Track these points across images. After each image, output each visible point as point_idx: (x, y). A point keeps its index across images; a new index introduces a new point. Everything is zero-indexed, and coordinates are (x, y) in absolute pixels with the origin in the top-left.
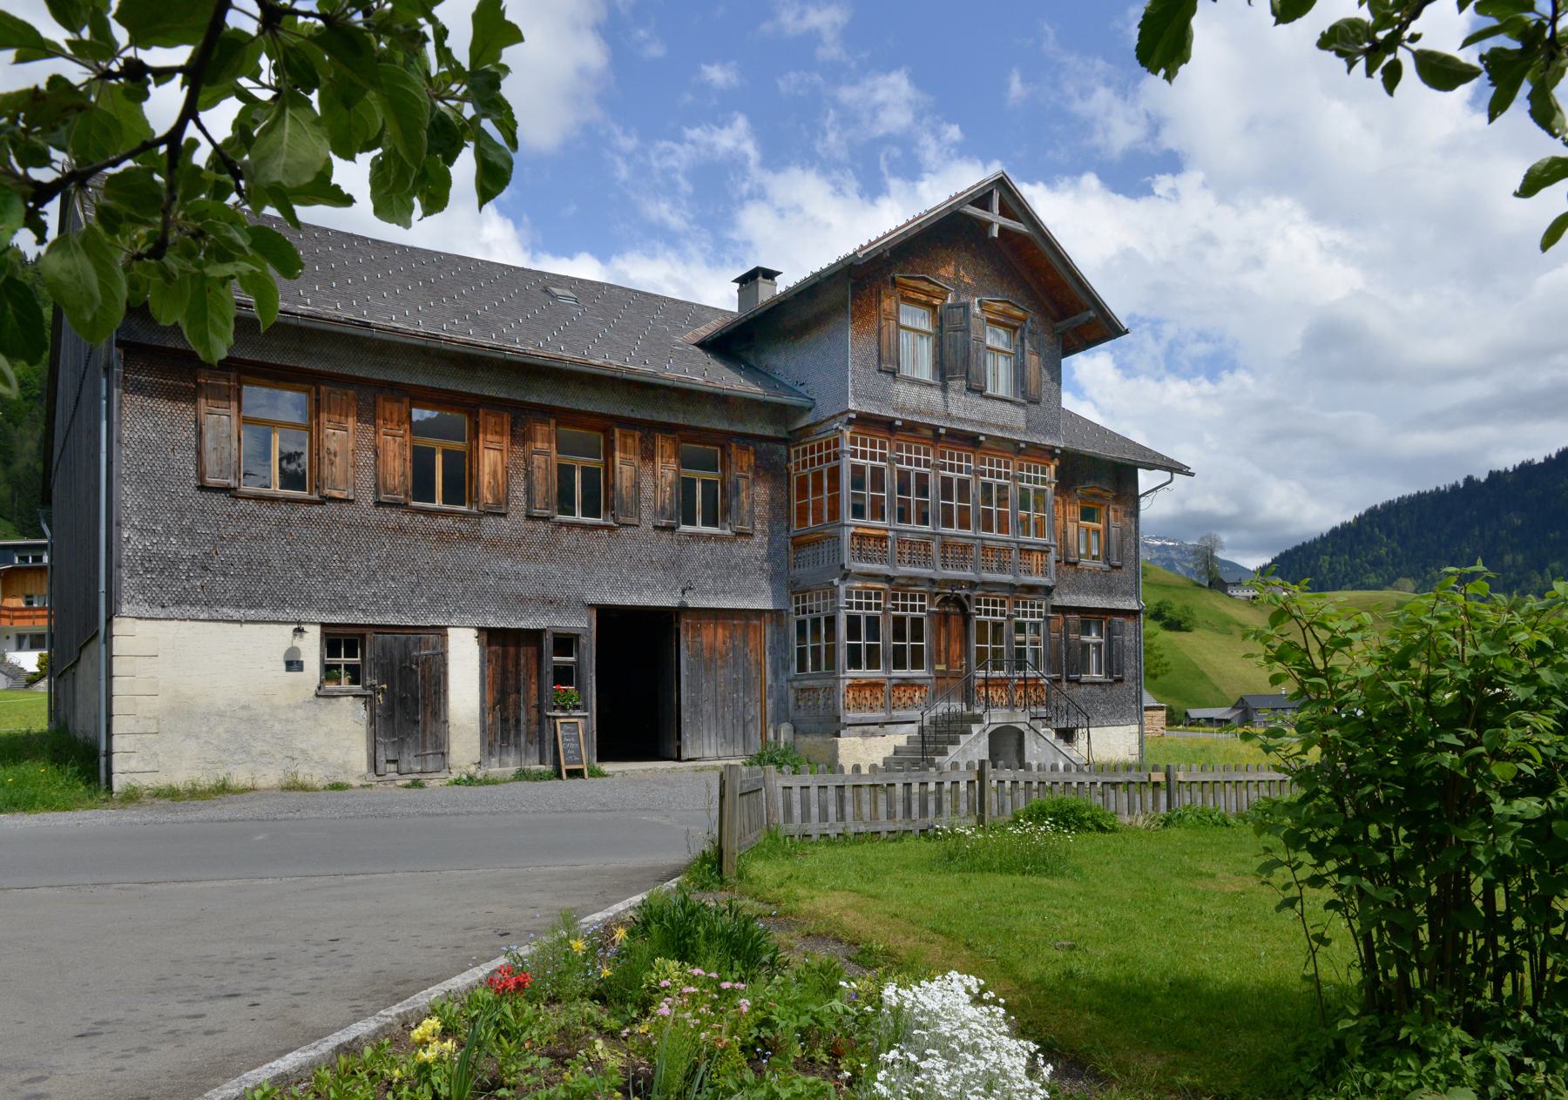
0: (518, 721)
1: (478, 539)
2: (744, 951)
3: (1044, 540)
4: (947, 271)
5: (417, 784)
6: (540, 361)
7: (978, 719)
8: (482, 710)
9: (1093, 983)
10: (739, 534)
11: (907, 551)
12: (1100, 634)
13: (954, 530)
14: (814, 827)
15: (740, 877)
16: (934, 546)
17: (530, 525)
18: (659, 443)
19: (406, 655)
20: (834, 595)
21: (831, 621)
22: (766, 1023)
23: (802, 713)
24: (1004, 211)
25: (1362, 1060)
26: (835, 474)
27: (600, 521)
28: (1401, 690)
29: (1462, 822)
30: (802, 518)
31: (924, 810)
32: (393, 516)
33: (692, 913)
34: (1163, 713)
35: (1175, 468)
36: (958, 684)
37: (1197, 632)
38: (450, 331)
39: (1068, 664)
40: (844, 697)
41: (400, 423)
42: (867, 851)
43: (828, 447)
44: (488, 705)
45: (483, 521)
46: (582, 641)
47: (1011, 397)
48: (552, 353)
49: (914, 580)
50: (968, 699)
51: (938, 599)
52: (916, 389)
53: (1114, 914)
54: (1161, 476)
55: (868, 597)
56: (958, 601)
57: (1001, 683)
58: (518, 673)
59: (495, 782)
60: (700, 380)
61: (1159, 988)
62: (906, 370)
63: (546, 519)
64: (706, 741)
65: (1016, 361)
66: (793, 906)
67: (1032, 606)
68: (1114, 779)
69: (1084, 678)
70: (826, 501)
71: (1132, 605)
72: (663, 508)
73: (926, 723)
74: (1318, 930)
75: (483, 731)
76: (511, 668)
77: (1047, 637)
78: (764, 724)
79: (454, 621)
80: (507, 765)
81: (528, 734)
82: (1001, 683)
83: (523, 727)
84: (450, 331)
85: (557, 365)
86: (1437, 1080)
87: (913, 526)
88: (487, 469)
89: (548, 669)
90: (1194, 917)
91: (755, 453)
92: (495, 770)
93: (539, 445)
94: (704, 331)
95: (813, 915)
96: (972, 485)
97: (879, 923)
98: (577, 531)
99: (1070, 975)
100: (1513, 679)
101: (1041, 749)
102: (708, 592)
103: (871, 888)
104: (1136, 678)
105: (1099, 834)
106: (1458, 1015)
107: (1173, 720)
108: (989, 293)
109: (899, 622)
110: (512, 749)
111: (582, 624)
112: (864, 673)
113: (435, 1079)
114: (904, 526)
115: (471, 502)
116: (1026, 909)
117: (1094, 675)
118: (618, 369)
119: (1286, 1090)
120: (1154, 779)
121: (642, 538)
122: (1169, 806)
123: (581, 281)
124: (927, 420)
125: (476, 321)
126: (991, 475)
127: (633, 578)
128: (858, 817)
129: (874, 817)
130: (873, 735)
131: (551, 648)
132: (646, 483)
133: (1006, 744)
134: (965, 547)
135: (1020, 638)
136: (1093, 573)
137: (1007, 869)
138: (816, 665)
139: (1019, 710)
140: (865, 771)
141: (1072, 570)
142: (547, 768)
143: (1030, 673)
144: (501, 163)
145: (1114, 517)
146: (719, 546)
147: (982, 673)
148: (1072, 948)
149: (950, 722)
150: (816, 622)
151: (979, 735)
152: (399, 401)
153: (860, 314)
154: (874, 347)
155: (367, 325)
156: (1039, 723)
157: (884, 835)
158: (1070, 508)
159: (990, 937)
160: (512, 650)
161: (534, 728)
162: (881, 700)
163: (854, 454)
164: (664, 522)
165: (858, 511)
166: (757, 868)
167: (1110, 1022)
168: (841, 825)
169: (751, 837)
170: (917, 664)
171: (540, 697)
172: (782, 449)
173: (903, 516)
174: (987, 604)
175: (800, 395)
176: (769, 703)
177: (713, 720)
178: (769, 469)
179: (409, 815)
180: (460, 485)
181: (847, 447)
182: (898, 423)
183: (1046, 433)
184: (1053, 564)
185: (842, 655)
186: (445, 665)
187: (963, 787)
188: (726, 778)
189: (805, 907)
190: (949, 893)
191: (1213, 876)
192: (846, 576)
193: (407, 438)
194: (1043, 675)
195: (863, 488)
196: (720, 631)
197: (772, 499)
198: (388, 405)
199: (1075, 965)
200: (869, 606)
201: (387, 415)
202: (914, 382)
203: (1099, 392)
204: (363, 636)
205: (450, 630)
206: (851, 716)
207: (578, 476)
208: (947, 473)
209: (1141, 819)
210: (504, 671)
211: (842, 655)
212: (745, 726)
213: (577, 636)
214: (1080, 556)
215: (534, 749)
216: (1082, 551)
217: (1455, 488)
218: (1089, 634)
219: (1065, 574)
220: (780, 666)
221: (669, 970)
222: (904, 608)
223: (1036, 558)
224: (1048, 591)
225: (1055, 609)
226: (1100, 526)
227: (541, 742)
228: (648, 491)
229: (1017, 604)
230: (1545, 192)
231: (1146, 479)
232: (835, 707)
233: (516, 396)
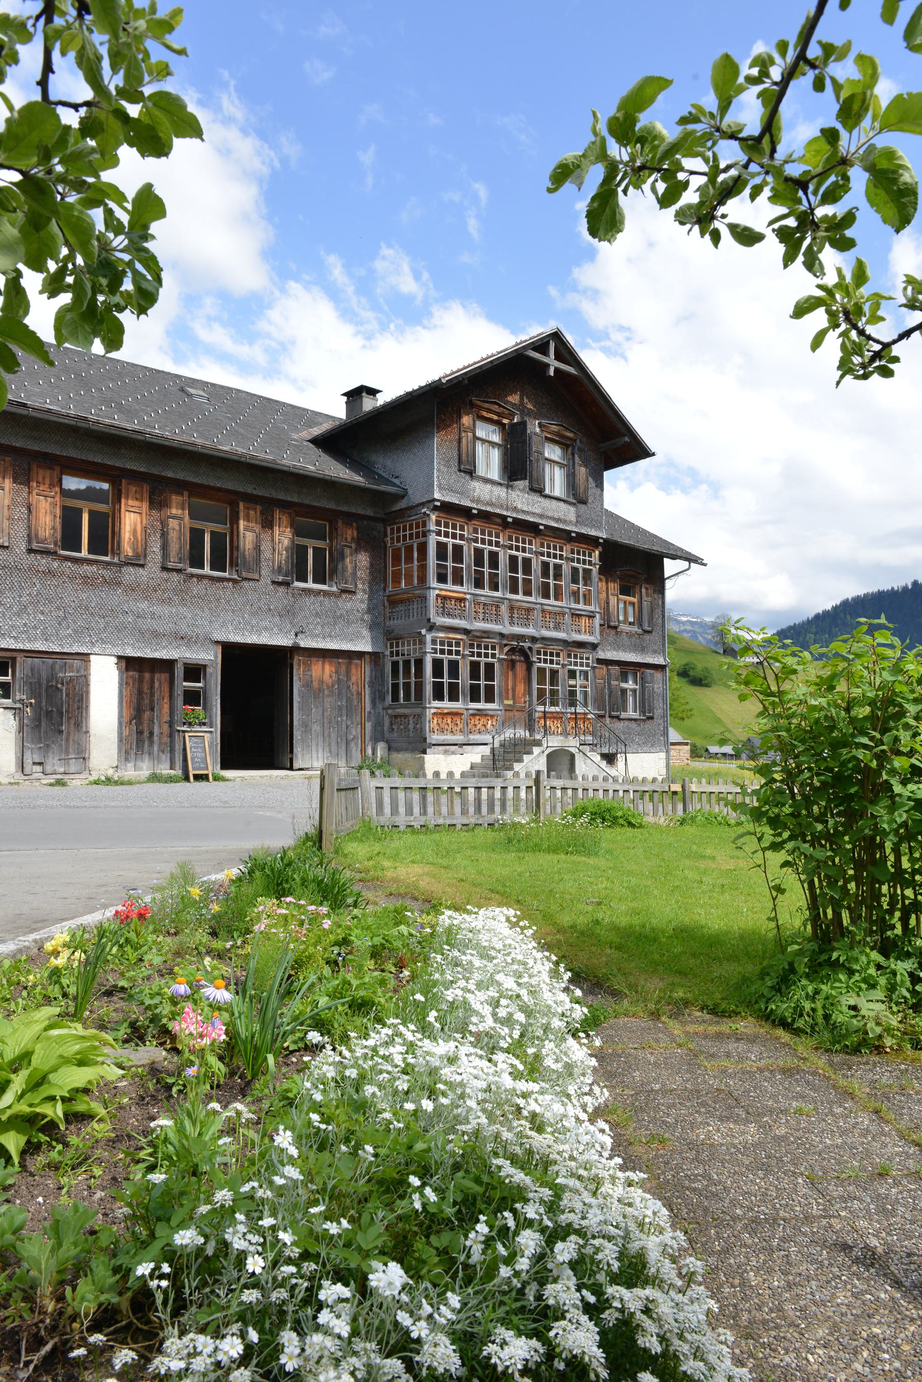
0: (151, 733)
1: (119, 584)
2: (332, 894)
3: (592, 608)
4: (514, 399)
5: (60, 783)
6: (175, 444)
7: (538, 743)
8: (120, 723)
9: (614, 928)
10: (344, 591)
11: (481, 611)
12: (635, 682)
13: (520, 597)
14: (402, 820)
15: (337, 852)
16: (504, 609)
17: (165, 575)
18: (277, 515)
19: (52, 676)
20: (422, 642)
21: (420, 663)
22: (345, 942)
23: (395, 735)
24: (558, 357)
25: (807, 976)
26: (423, 548)
27: (226, 575)
28: (829, 704)
29: (873, 802)
30: (397, 581)
31: (491, 809)
32: (43, 562)
33: (289, 864)
34: (688, 748)
35: (692, 559)
36: (524, 715)
37: (715, 688)
38: (98, 415)
39: (610, 705)
40: (431, 723)
41: (52, 486)
42: (445, 838)
43: (418, 527)
44: (125, 720)
45: (124, 569)
46: (209, 670)
47: (563, 497)
48: (185, 438)
49: (487, 634)
50: (531, 728)
51: (506, 649)
52: (489, 486)
53: (634, 881)
54: (682, 564)
55: (450, 645)
56: (522, 651)
57: (557, 716)
58: (152, 694)
59: (130, 783)
60: (312, 468)
61: (663, 932)
62: (481, 471)
63: (179, 571)
64: (314, 755)
65: (568, 470)
67: (582, 658)
68: (647, 793)
69: (623, 715)
70: (415, 568)
71: (659, 660)
72: (280, 567)
73: (497, 745)
74: (777, 882)
75: (120, 740)
76: (146, 689)
78: (363, 742)
79: (96, 650)
80: (141, 769)
81: (160, 743)
82: (557, 716)
83: (156, 739)
84: (98, 415)
85: (190, 448)
86: (860, 988)
87: (486, 591)
88: (128, 528)
90: (695, 885)
91: (357, 529)
92: (129, 772)
93: (174, 511)
94: (316, 431)
95: (395, 880)
96: (534, 562)
97: (449, 885)
98: (205, 581)
99: (597, 922)
100: (908, 700)
101: (589, 766)
102: (317, 636)
103: (444, 862)
104: (664, 716)
105: (630, 829)
106: (876, 942)
107: (695, 753)
108: (548, 418)
109: (475, 666)
110: (146, 757)
111: (210, 657)
113: (65, 981)
114: (479, 591)
115: (113, 553)
116: (566, 877)
117: (631, 713)
118: (242, 455)
119: (753, 1001)
120: (673, 789)
121: (262, 590)
122: (685, 810)
123: (213, 385)
124: (498, 511)
125: (120, 408)
126: (549, 556)
127: (254, 622)
128: (437, 812)
129: (451, 813)
130: (453, 753)
131: (182, 675)
132: (266, 547)
133: (560, 762)
134: (528, 610)
135: (572, 682)
136: (630, 635)
137: (554, 850)
138: (407, 697)
140: (443, 776)
141: (613, 632)
142: (178, 772)
143: (580, 709)
144: (150, 288)
145: (646, 594)
146: (326, 600)
148: (599, 904)
149: (515, 745)
150: (407, 663)
151: (539, 755)
152: (51, 468)
153: (443, 425)
154: (455, 453)
155: (24, 405)
156: (588, 748)
157: (459, 827)
158: (611, 585)
159: (536, 895)
160: (147, 676)
161: (166, 739)
162: (460, 726)
163: (439, 533)
164: (281, 578)
165: (442, 578)
166: (351, 847)
167: (625, 956)
168: (423, 818)
169: (348, 825)
170: (490, 699)
171: (172, 714)
172: (380, 526)
173: (479, 584)
174: (545, 654)
175: (395, 485)
176: (368, 725)
177: (320, 738)
178: (371, 541)
179: (52, 807)
180: (104, 538)
181: (433, 527)
182: (475, 512)
183: (593, 526)
184: (598, 626)
185: (429, 689)
187: (523, 794)
188: (326, 774)
189: (389, 874)
190: (507, 866)
191: (714, 858)
192: (432, 628)
193: (58, 499)
194: (591, 712)
195: (446, 560)
196: (327, 667)
197: (372, 565)
198: (41, 472)
199: (600, 916)
200: (450, 652)
201: (40, 479)
202: (487, 481)
203: (631, 498)
204: (14, 659)
205: (92, 657)
206: (435, 737)
207: (207, 538)
208: (514, 552)
209: (662, 819)
210: (140, 692)
211: (429, 689)
212: (347, 744)
213: (205, 666)
214: (619, 621)
215: (165, 757)
216: (621, 618)
217: (905, 589)
218: (626, 682)
220: (378, 696)
221: (265, 904)
222: (479, 655)
223: (584, 621)
224: (594, 646)
225: (600, 661)
226: (635, 600)
227: (172, 751)
228: (266, 554)
229: (569, 656)
230: (807, 317)
231: (670, 566)
232: (422, 730)
233: (155, 471)
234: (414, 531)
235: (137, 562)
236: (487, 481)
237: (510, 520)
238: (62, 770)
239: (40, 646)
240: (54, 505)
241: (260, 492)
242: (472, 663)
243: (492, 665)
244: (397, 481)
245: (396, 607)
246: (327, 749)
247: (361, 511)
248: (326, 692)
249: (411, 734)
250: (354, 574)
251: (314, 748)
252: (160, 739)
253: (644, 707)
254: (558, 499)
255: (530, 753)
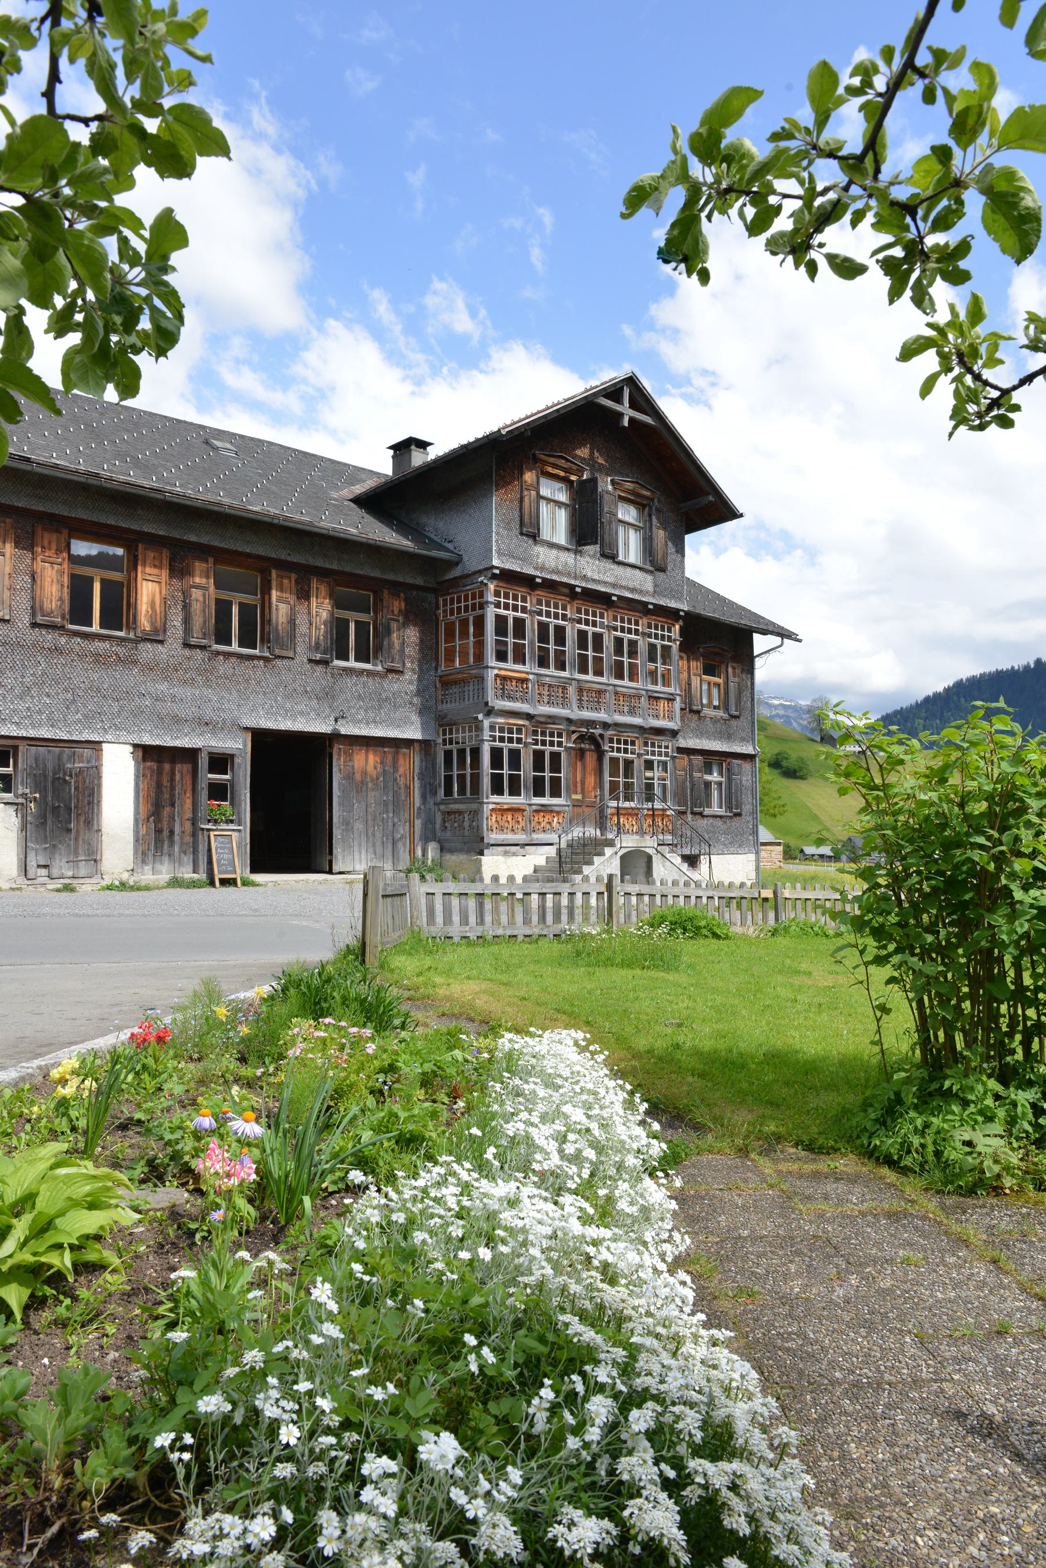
0: (172, 832)
1: (135, 662)
2: (377, 1014)
3: (671, 690)
4: (583, 452)
5: (68, 888)
6: (199, 504)
7: (611, 843)
8: (136, 821)
9: (697, 1053)
10: (390, 671)
11: (546, 693)
12: (721, 774)
13: (590, 677)
14: (456, 930)
15: (382, 967)
16: (572, 690)
17: (187, 652)
18: (314, 584)
19: (59, 767)
20: (479, 728)
21: (476, 752)
22: (391, 1069)
23: (449, 834)
24: (633, 405)
25: (916, 1107)
26: (480, 622)
27: (257, 652)
28: (940, 799)
30: (450, 659)
32: (49, 638)
33: (328, 981)
34: (780, 848)
35: (784, 634)
36: (594, 812)
37: (811, 780)
38: (111, 471)
39: (692, 800)
40: (489, 820)
41: (59, 551)
42: (505, 951)
45: (141, 646)
46: (237, 760)
47: (639, 563)
48: (210, 497)
49: (552, 719)
50: (602, 826)
51: (574, 736)
52: (554, 552)
53: (719, 1000)
54: (774, 640)
55: (511, 731)
56: (592, 739)
57: (632, 813)
58: (172, 788)
59: (147, 888)
60: (354, 531)
61: (752, 1057)
62: (545, 534)
63: (203, 648)
64: (357, 857)
66: (431, 991)
67: (660, 747)
68: (735, 900)
69: (707, 811)
70: (471, 644)
71: (748, 749)
72: (317, 644)
73: (563, 845)
74: (882, 1000)
75: (137, 840)
76: (166, 783)
77: (675, 778)
78: (412, 842)
80: (160, 873)
82: (632, 813)
83: (177, 838)
84: (111, 471)
85: (216, 508)
86: (976, 1121)
87: (552, 671)
88: (145, 599)
89: (203, 786)
90: (789, 1004)
91: (405, 600)
92: (147, 876)
93: (197, 580)
94: (359, 489)
95: (448, 998)
96: (606, 638)
97: (509, 1004)
98: (233, 660)
99: (677, 1046)
100: (1030, 794)
101: (668, 869)
102: (360, 721)
103: (504, 978)
104: (753, 813)
105: (715, 941)
106: (993, 1069)
107: (789, 855)
108: (621, 474)
109: (539, 756)
110: (166, 858)
111: (238, 745)
112: (506, 799)
113: (73, 1113)
114: (543, 671)
115: (128, 628)
116: (642, 995)
117: (715, 809)
118: (274, 517)
119: (855, 1135)
120: (763, 895)
122: (777, 919)
123: (242, 437)
124: (565, 580)
125: (137, 463)
126: (623, 631)
127: (288, 705)
128: (496, 922)
129: (512, 922)
130: (514, 854)
131: (206, 766)
132: (301, 620)
133: (636, 864)
134: (600, 692)
135: (649, 774)
136: (714, 720)
137: (628, 964)
138: (462, 791)
139: (648, 837)
140: (503, 880)
141: (695, 717)
142: (202, 876)
143: (658, 805)
144: (170, 327)
145: (733, 674)
146: (370, 681)
147: (614, 804)
148: (680, 1025)
149: (585, 845)
150: (462, 752)
152: (58, 531)
153: (503, 483)
154: (517, 514)
155: (28, 460)
156: (666, 849)
157: (521, 938)
158: (693, 664)
159: (608, 1016)
160: (167, 766)
161: (188, 839)
162: (522, 824)
163: (498, 605)
164: (318, 656)
165: (501, 656)
166: (399, 961)
167: (709, 1084)
168: (480, 928)
170: (556, 793)
171: (195, 810)
172: (431, 597)
173: (543, 662)
174: (619, 742)
175: (448, 550)
176: (418, 823)
177: (364, 838)
178: (421, 614)
179: (59, 915)
180: (118, 610)
182: (539, 580)
183: (673, 597)
184: (678, 711)
185: (486, 782)
186: (99, 777)
187: (593, 901)
188: (370, 878)
189: (441, 992)
190: (574, 982)
191: (810, 974)
192: (490, 712)
193: (65, 566)
194: (671, 808)
195: (506, 636)
196: (371, 757)
197: (422, 641)
198: (46, 535)
199: (681, 1039)
200: (511, 740)
201: (46, 544)
202: (552, 545)
203: (716, 565)
204: (16, 748)
205: (105, 746)
206: (493, 837)
207: (235, 610)
208: (583, 627)
209: (752, 930)
210: (159, 786)
211: (486, 782)
212: (394, 844)
213: (232, 756)
215: (188, 859)
216: (705, 701)
217: (1027, 668)
218: (711, 773)
219: (690, 721)
220: (429, 790)
222: (544, 743)
223: (662, 705)
224: (674, 734)
225: (680, 750)
227: (195, 852)
228: (302, 628)
229: (646, 744)
230: (915, 360)
231: (760, 643)
232: (479, 828)
233: (176, 534)
234: (470, 602)
235: (156, 637)
236: (552, 545)
237: (578, 590)
238: (70, 874)
239: (45, 733)
240: (61, 573)
241: (295, 558)
242: (535, 752)
243: (558, 754)
244: (450, 546)
245: (449, 689)
246: (371, 850)
247: (409, 580)
248: (370, 785)
249: (467, 833)
250: (402, 651)
251: (356, 849)
252: (182, 838)
253: (730, 802)
254: (633, 566)
255: (601, 854)
